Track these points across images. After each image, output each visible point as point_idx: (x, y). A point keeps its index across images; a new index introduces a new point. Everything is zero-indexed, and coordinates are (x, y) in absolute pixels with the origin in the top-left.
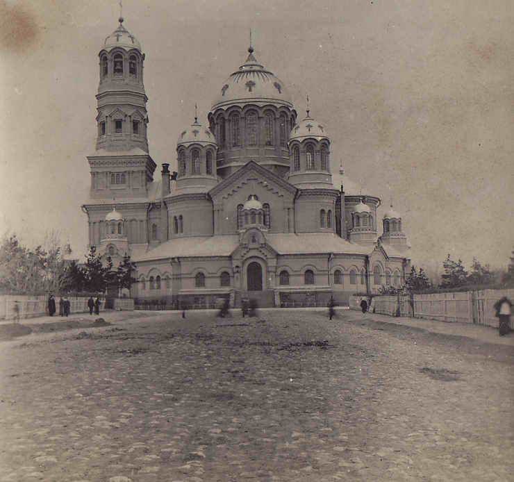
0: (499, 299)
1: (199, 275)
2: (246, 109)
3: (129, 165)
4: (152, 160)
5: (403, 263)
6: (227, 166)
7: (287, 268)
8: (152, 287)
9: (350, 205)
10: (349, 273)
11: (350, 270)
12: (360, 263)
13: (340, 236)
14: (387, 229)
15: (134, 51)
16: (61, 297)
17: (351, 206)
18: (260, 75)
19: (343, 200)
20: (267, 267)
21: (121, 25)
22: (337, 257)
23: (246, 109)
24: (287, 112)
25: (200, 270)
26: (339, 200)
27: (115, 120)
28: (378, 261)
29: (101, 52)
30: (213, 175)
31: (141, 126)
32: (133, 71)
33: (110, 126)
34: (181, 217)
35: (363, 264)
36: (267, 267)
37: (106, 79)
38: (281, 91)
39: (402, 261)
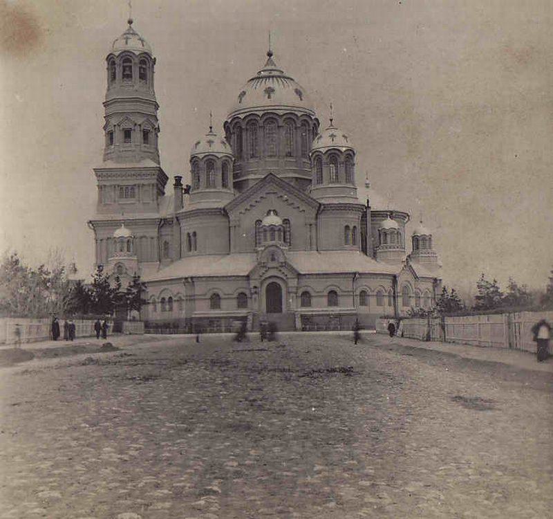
0: (538, 322)
2: (265, 118)
5: (434, 283)
8: (164, 310)
9: (381, 220)
10: (375, 293)
11: (376, 291)
12: (387, 283)
13: (366, 255)
20: (287, 287)
23: (265, 118)
26: (364, 216)
27: (123, 129)
28: (406, 281)
29: (108, 56)
30: (229, 189)
31: (151, 136)
32: (143, 76)
33: (118, 136)
34: (195, 234)
35: (391, 285)
36: (287, 287)
37: (114, 85)
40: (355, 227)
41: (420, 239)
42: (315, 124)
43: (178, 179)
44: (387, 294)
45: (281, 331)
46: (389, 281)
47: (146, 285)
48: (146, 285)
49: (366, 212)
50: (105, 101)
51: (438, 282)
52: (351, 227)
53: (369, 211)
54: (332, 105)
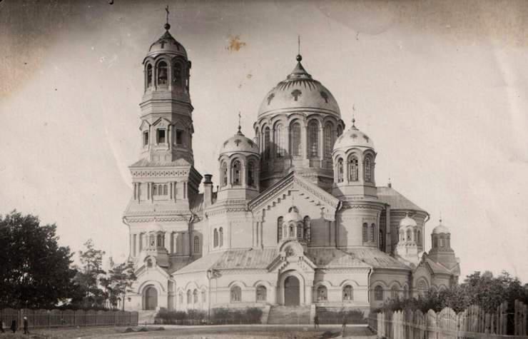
0: (235, 336)
1: (260, 289)
2: (310, 119)
3: (171, 176)
4: (198, 173)
5: (450, 279)
6: (267, 178)
7: (345, 283)
8: (189, 301)
9: (397, 218)
10: (390, 288)
11: (391, 286)
12: (403, 279)
13: (385, 252)
14: (435, 244)
15: (180, 59)
16: (115, 310)
17: (397, 221)
18: (307, 84)
19: (388, 214)
21: (167, 32)
22: (379, 272)
23: (310, 119)
24: (334, 122)
25: (260, 283)
26: (383, 214)
27: (158, 129)
28: (393, 281)
29: (145, 60)
30: (255, 187)
31: (185, 137)
33: (153, 136)
34: (221, 229)
35: (407, 280)
37: (149, 88)
38: (271, 103)
39: (449, 277)
40: (373, 224)
41: (439, 237)
42: (339, 125)
43: (209, 177)
44: (403, 289)
45: (322, 324)
46: (405, 276)
47: (220, 273)
48: (220, 273)
49: (385, 210)
50: (141, 102)
51: (455, 278)
52: (369, 225)
53: (388, 210)
54: (355, 107)
